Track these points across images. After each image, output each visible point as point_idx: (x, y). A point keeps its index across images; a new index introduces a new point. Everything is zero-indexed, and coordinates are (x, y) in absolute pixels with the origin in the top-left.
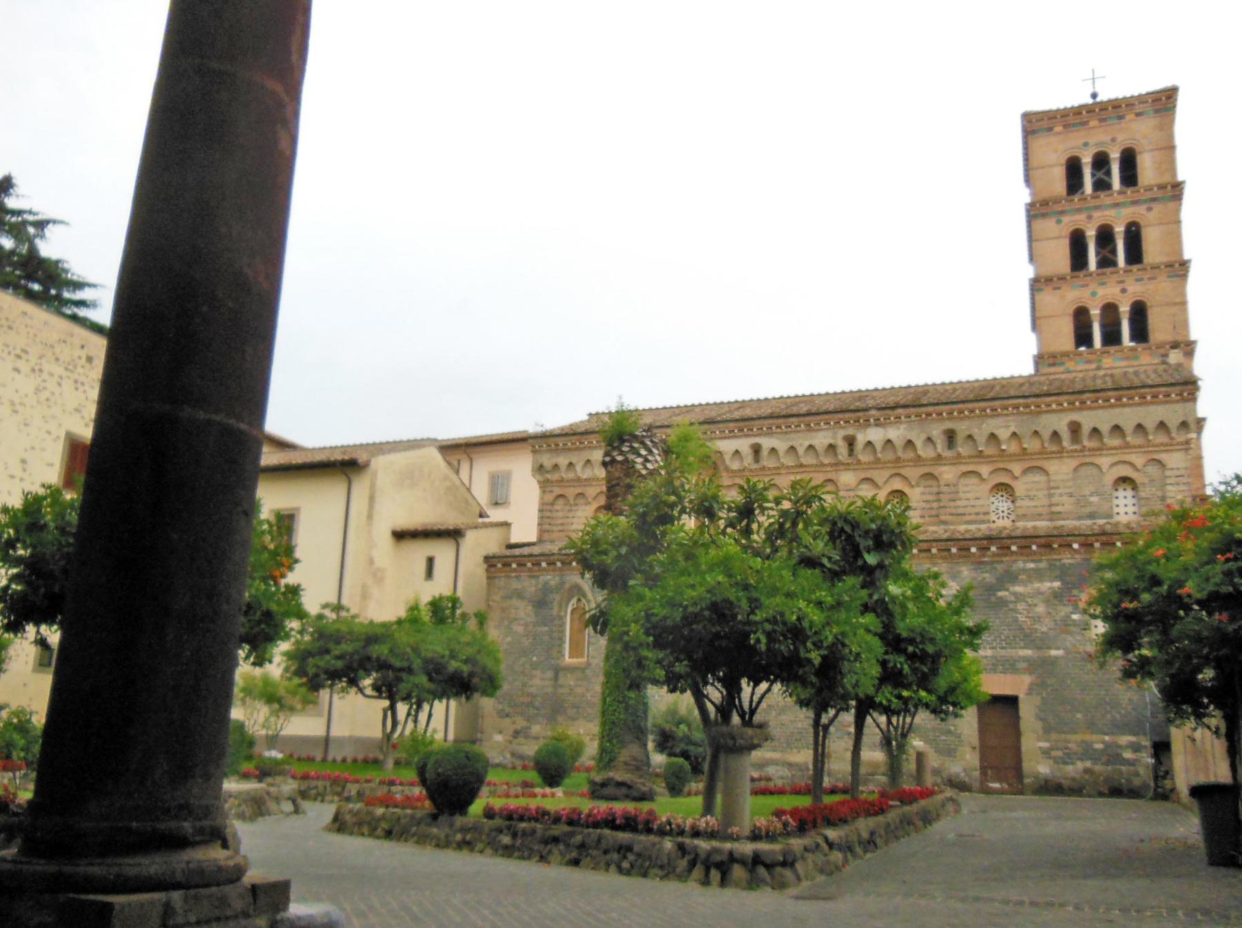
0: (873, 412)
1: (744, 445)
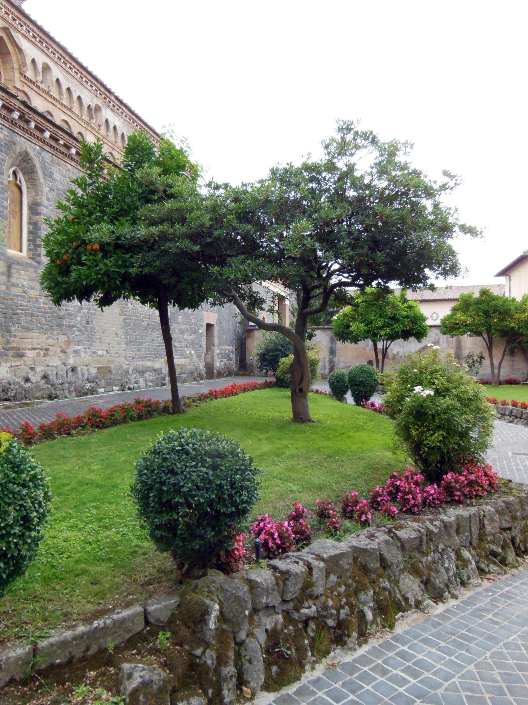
0: (113, 98)
1: (41, 59)
